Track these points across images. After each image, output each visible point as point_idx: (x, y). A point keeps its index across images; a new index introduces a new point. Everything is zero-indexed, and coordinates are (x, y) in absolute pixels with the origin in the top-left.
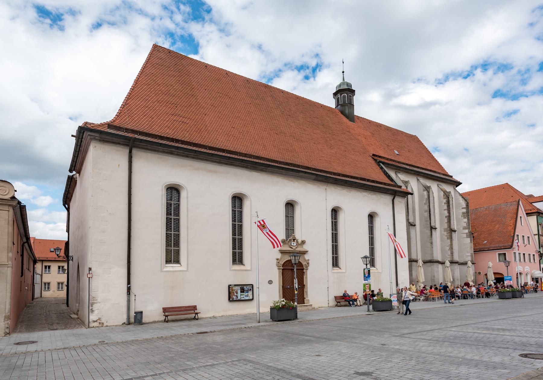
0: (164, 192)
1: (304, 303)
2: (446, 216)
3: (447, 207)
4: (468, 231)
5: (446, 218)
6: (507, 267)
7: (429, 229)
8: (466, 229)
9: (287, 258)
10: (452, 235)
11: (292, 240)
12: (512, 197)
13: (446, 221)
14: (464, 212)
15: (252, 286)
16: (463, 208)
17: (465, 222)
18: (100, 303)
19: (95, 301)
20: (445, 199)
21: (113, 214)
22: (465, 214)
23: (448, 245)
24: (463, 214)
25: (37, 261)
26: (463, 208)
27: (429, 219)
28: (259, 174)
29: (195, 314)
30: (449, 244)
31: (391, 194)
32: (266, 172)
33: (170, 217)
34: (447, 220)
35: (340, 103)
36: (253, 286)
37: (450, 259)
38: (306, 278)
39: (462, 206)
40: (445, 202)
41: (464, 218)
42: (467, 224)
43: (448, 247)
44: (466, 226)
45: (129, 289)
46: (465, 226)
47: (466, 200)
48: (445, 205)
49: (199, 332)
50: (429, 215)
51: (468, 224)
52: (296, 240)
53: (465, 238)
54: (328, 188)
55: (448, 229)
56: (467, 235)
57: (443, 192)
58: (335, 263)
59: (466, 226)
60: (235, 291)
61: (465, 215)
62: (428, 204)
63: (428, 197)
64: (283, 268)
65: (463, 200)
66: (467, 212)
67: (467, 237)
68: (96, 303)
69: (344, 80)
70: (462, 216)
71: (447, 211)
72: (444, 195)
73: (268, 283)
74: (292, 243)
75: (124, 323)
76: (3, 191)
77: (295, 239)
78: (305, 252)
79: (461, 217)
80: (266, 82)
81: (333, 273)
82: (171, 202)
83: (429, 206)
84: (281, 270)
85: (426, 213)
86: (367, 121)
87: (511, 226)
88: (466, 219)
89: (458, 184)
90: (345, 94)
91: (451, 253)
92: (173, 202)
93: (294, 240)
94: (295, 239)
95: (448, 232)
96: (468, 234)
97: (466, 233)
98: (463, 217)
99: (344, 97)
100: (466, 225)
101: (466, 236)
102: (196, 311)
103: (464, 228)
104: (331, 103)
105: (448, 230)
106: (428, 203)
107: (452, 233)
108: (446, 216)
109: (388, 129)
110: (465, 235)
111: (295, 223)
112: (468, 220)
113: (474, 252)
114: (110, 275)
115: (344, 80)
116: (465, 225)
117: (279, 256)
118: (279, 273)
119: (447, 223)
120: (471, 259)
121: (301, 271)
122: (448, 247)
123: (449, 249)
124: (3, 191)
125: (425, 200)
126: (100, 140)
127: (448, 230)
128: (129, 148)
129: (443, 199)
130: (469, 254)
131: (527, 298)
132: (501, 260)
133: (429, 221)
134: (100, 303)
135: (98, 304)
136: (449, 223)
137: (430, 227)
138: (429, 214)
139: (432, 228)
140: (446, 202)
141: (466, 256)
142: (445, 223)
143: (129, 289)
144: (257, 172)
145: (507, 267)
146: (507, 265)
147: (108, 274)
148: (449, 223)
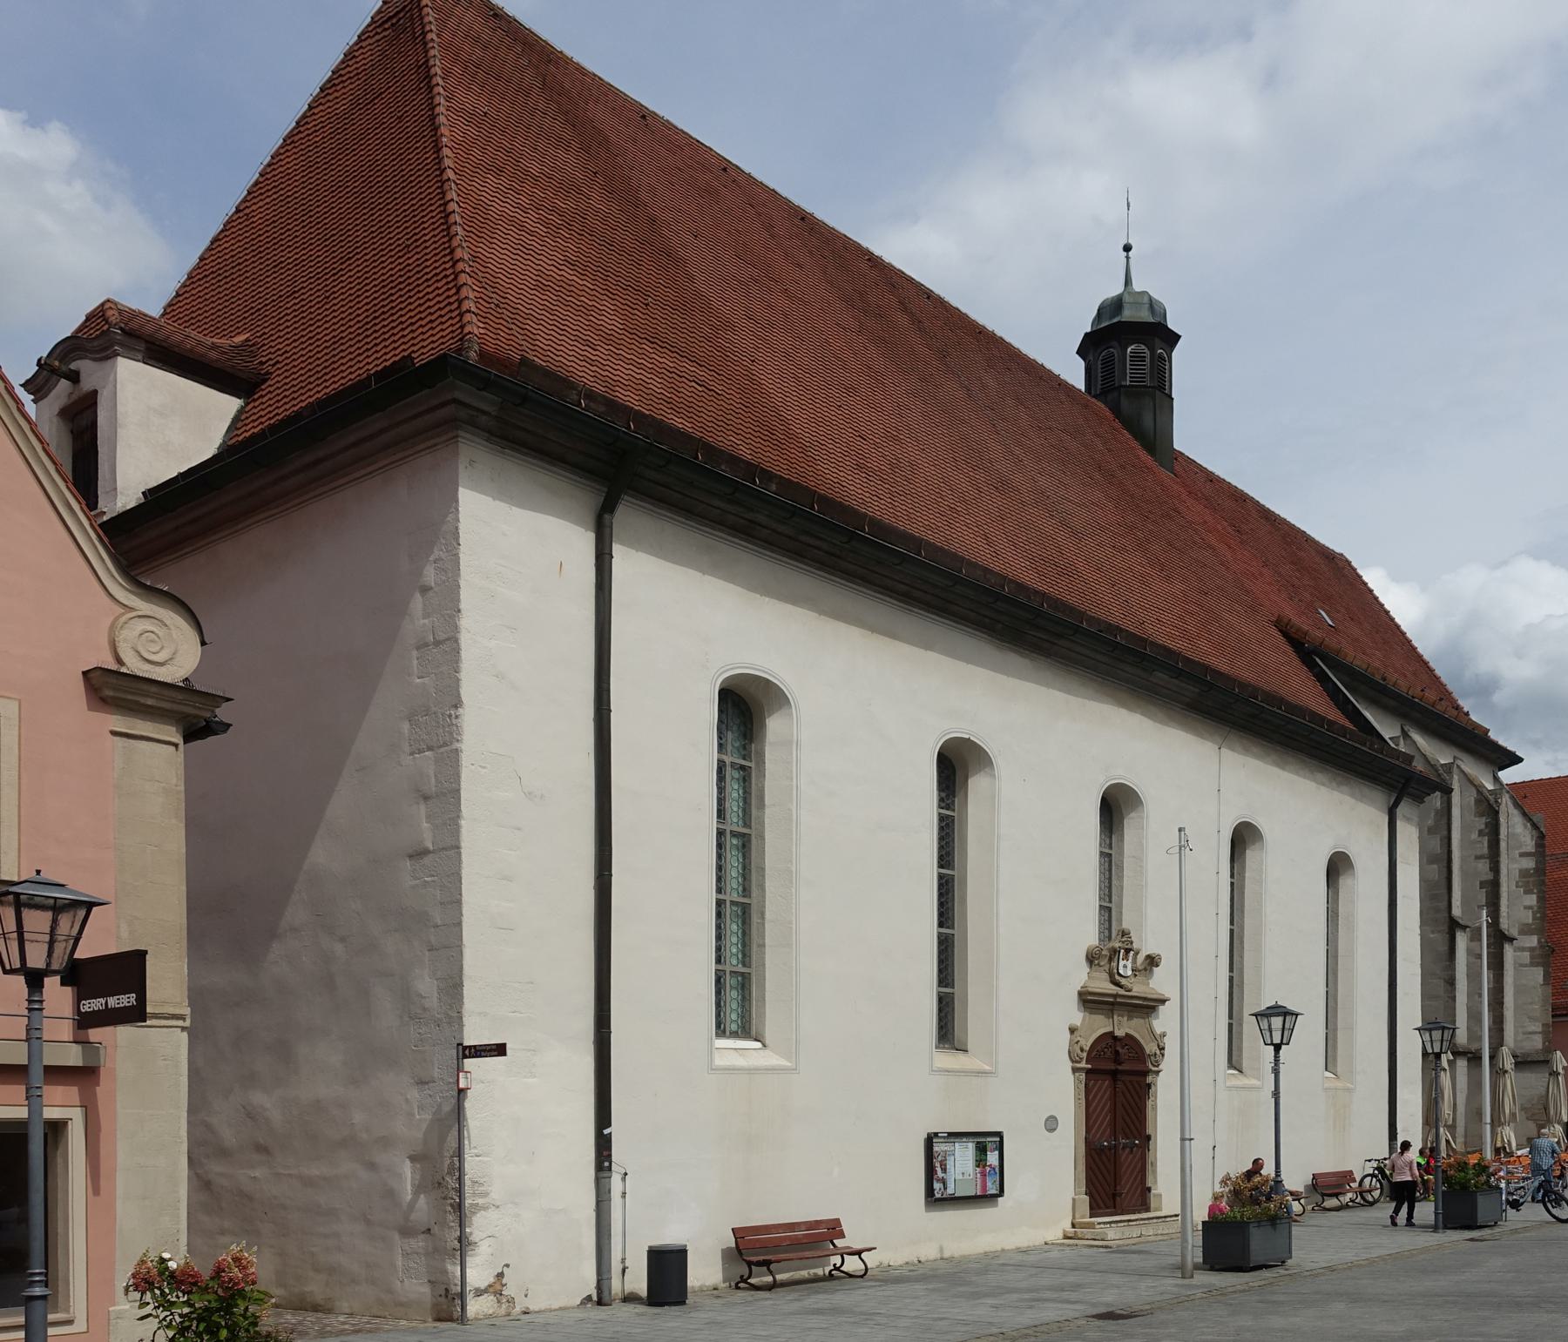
1: (1148, 1210)
3: (1489, 847)
4: (1539, 941)
5: (1484, 890)
6: (1277, 1048)
7: (1445, 928)
9: (1101, 1025)
11: (1122, 951)
14: (1527, 870)
15: (998, 1139)
16: (1522, 855)
17: (1530, 908)
18: (498, 1207)
19: (480, 1201)
20: (1481, 815)
21: (542, 796)
22: (1531, 875)
24: (1524, 877)
26: (1522, 855)
27: (1445, 891)
28: (1027, 661)
36: (1002, 1138)
38: (1155, 1108)
39: (1521, 847)
40: (1483, 827)
41: (1526, 892)
44: (1530, 921)
45: (603, 1146)
46: (1526, 921)
47: (1535, 826)
48: (1480, 839)
50: (1445, 874)
51: (1538, 915)
52: (1132, 953)
53: (1526, 966)
56: (1532, 957)
57: (1475, 792)
58: (948, 1031)
60: (940, 1158)
61: (1531, 879)
62: (1445, 833)
63: (1445, 805)
64: (1090, 1066)
65: (1526, 827)
66: (1540, 870)
67: (1532, 964)
68: (485, 1208)
69: (1128, 281)
70: (1517, 882)
71: (1488, 861)
73: (1047, 1120)
74: (1122, 963)
75: (589, 1298)
76: (152, 641)
77: (1131, 950)
79: (1514, 888)
83: (1446, 841)
84: (1083, 1076)
85: (1435, 866)
86: (1201, 470)
88: (1534, 897)
92: (731, 759)
93: (1127, 951)
94: (1131, 950)
97: (1532, 949)
98: (1522, 890)
101: (1528, 961)
103: (1526, 930)
104: (1074, 373)
106: (1446, 827)
108: (1481, 883)
109: (74, 462)
110: (1527, 954)
112: (1541, 899)
113: (1553, 1016)
114: (530, 1080)
115: (1128, 281)
116: (1528, 918)
117: (1077, 1017)
118: (1076, 1088)
120: (1544, 1043)
121: (1130, 1081)
124: (152, 641)
125: (1433, 814)
126: (489, 432)
128: (606, 490)
129: (1472, 817)
130: (1538, 1027)
133: (1446, 898)
134: (498, 1207)
135: (492, 1214)
136: (1492, 909)
137: (1447, 919)
138: (1445, 870)
139: (1453, 926)
141: (1524, 1033)
143: (603, 1146)
144: (1021, 655)
145: (1277, 1048)
146: (1277, 1040)
147: (525, 1077)
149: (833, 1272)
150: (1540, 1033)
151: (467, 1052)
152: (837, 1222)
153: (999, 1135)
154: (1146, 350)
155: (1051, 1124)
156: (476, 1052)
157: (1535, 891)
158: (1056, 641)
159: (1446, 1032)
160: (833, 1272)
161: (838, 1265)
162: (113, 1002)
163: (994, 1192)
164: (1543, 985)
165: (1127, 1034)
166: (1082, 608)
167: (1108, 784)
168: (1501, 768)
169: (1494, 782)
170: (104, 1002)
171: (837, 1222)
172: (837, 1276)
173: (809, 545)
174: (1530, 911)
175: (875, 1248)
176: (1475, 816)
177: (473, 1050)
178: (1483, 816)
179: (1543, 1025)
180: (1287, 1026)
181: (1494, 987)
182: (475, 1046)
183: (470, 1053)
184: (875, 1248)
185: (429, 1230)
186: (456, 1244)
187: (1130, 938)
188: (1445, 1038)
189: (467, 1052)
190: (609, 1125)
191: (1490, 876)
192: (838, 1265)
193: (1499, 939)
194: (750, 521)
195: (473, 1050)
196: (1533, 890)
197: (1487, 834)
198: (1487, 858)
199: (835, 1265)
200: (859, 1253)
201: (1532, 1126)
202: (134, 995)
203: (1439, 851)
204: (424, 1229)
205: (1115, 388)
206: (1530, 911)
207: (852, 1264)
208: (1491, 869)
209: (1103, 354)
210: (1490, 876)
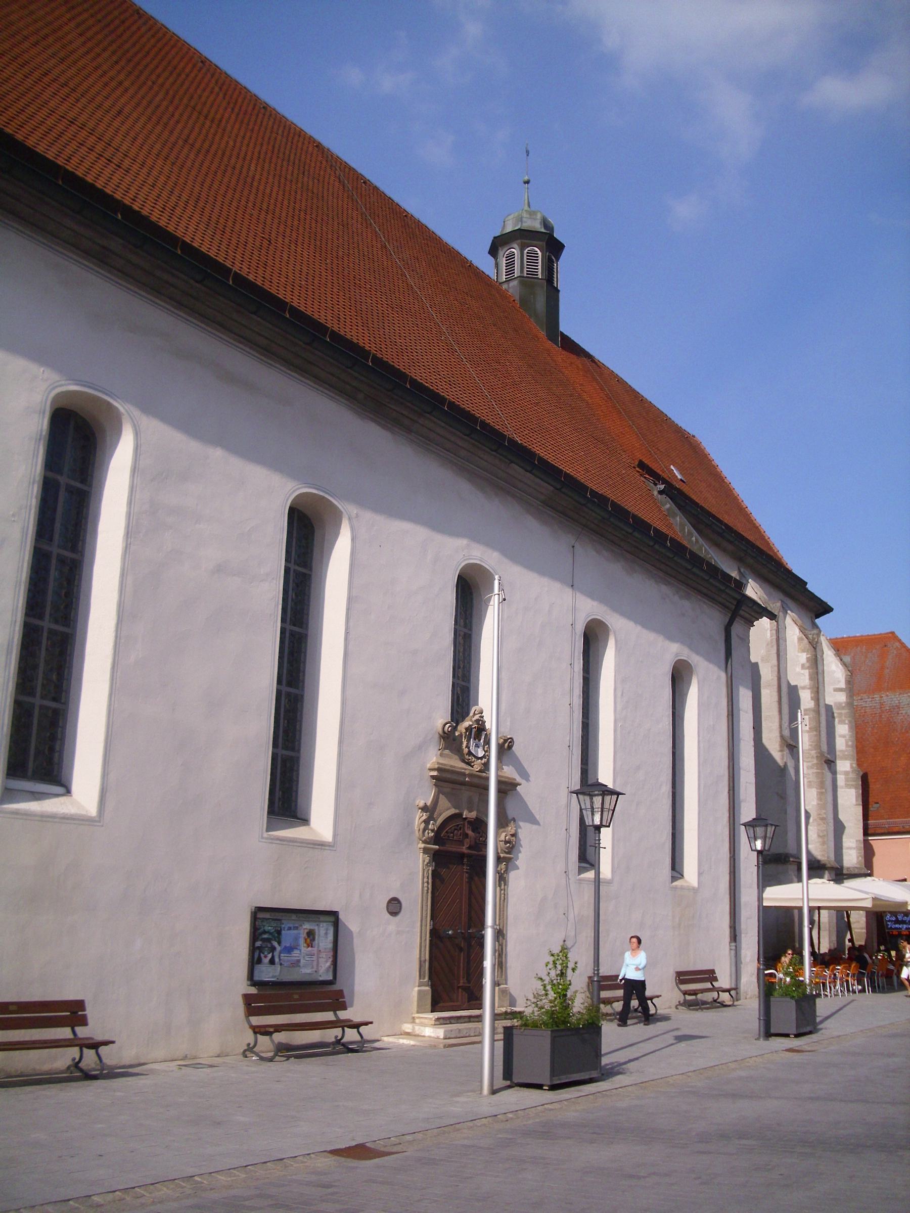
3: (811, 679)
8: (846, 759)
20: (803, 651)
22: (843, 708)
25: (622, 999)
26: (836, 690)
29: (77, 1049)
32: (409, 430)
33: (45, 547)
35: (517, 273)
42: (847, 742)
48: (803, 671)
54: (579, 549)
55: (813, 752)
56: (847, 780)
61: (843, 711)
62: (775, 662)
63: (775, 637)
72: (800, 639)
81: (580, 880)
82: (59, 477)
83: (776, 668)
88: (846, 727)
89: (822, 609)
90: (536, 249)
100: (844, 745)
102: (81, 1032)
105: (813, 757)
132: (276, 809)
140: (807, 661)
150: (854, 848)
152: (79, 1005)
155: (394, 906)
157: (847, 722)
159: (769, 829)
166: (835, 933)
167: (463, 564)
168: (818, 616)
169: (812, 625)
171: (79, 1005)
172: (342, 1048)
175: (371, 1023)
176: (799, 652)
178: (805, 652)
179: (857, 841)
180: (606, 806)
181: (818, 804)
184: (371, 1023)
186: (544, 992)
187: (483, 717)
188: (768, 835)
194: (104, 247)
196: (844, 721)
197: (808, 668)
198: (809, 689)
199: (249, 1044)
200: (357, 1026)
203: (771, 678)
207: (351, 1035)
209: (507, 253)
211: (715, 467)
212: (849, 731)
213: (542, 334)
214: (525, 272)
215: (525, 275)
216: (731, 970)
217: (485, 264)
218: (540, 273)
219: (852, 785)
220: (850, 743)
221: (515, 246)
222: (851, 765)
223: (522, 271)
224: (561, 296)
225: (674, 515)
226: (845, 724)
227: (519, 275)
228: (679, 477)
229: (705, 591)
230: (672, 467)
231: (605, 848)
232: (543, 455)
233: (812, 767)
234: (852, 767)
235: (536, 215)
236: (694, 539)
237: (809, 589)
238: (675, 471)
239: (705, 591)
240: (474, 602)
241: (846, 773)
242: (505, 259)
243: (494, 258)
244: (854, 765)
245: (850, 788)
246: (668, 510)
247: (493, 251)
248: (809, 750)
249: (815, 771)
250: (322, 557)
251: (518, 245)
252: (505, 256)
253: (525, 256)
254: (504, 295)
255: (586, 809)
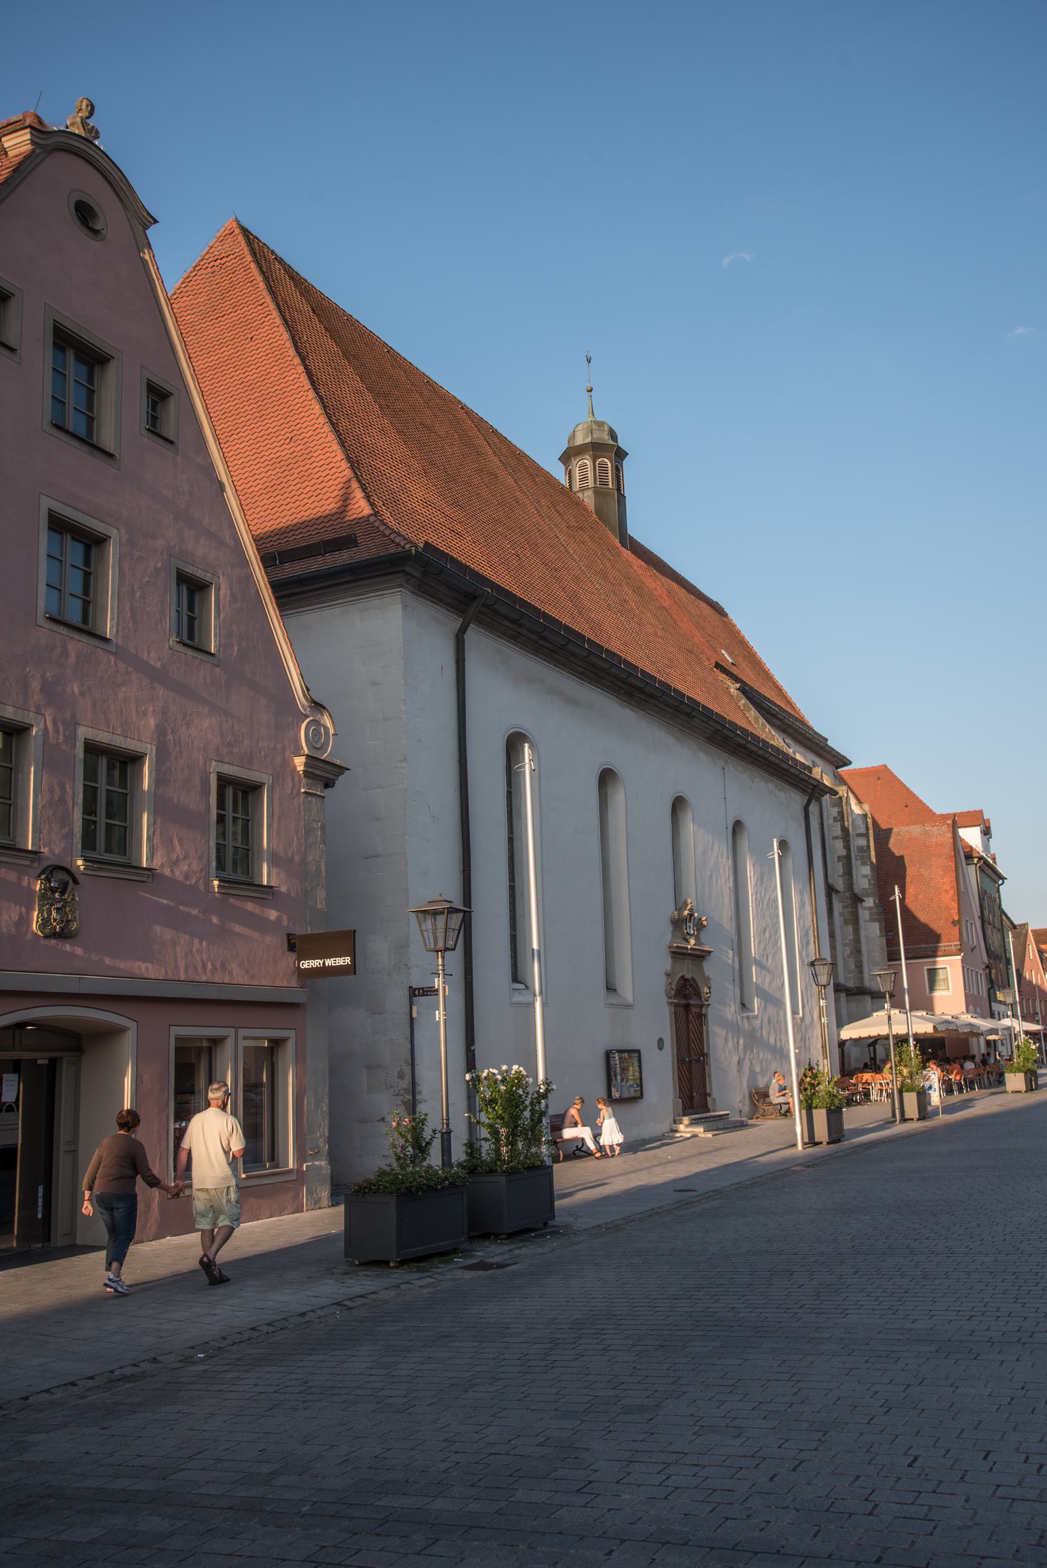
0: (980, 809)
2: (839, 857)
5: (841, 863)
10: (857, 912)
12: (906, 806)
13: (841, 872)
23: (847, 941)
30: (851, 937)
31: (803, 791)
34: (843, 869)
37: (855, 983)
42: (869, 881)
43: (848, 948)
44: (867, 886)
46: (864, 887)
48: (835, 824)
49: (605, 1186)
55: (847, 894)
56: (871, 914)
59: (867, 886)
67: (872, 920)
78: (704, 954)
80: (583, 440)
87: (947, 891)
90: (606, 460)
91: (856, 966)
95: (845, 904)
96: (874, 910)
99: (603, 468)
100: (867, 884)
105: (847, 898)
107: (857, 908)
111: (515, 866)
119: (842, 876)
122: (848, 948)
123: (851, 953)
127: (847, 898)
131: (128, 1366)
136: (847, 877)
142: (839, 876)
148: (847, 877)
149: (576, 1152)
151: (417, 992)
153: (638, 1052)
154: (609, 463)
156: (424, 992)
158: (648, 700)
160: (576, 1152)
161: (580, 1147)
162: (329, 962)
163: (633, 1094)
164: (880, 936)
165: (693, 979)
170: (321, 963)
173: (543, 646)
174: (867, 879)
177: (421, 991)
181: (854, 938)
182: (423, 989)
183: (419, 993)
185: (384, 1119)
189: (417, 992)
190: (473, 1044)
191: (844, 853)
192: (580, 1147)
193: (857, 899)
194: (519, 633)
195: (421, 991)
199: (577, 1146)
201: (550, 1088)
202: (349, 958)
204: (379, 1118)
205: (589, 488)
206: (867, 879)
208: (844, 847)
209: (579, 463)
210: (844, 853)
211: (739, 632)
212: (871, 872)
213: (617, 542)
214: (598, 483)
215: (598, 486)
216: (711, 1085)
217: (558, 473)
218: (610, 483)
219: (876, 919)
220: (872, 882)
221: (588, 457)
222: (874, 901)
223: (595, 482)
224: (627, 501)
225: (749, 710)
226: (868, 865)
227: (593, 486)
228: (730, 661)
229: (792, 781)
230: (723, 652)
231: (451, 975)
232: (485, 573)
233: (847, 907)
234: (875, 903)
235: (604, 427)
236: (767, 730)
237: (830, 745)
238: (726, 655)
239: (792, 781)
240: (609, 801)
241: (870, 909)
242: (577, 469)
243: (565, 464)
244: (877, 901)
245: (874, 922)
246: (744, 705)
247: (566, 458)
248: (844, 891)
249: (850, 910)
250: (607, 809)
251: (590, 456)
252: (578, 466)
253: (597, 468)
254: (579, 504)
255: (427, 930)
